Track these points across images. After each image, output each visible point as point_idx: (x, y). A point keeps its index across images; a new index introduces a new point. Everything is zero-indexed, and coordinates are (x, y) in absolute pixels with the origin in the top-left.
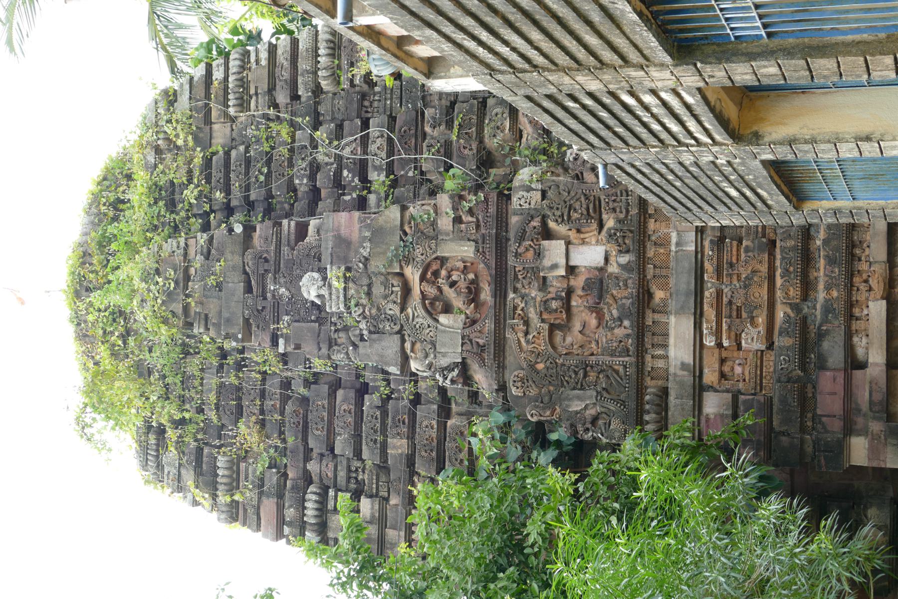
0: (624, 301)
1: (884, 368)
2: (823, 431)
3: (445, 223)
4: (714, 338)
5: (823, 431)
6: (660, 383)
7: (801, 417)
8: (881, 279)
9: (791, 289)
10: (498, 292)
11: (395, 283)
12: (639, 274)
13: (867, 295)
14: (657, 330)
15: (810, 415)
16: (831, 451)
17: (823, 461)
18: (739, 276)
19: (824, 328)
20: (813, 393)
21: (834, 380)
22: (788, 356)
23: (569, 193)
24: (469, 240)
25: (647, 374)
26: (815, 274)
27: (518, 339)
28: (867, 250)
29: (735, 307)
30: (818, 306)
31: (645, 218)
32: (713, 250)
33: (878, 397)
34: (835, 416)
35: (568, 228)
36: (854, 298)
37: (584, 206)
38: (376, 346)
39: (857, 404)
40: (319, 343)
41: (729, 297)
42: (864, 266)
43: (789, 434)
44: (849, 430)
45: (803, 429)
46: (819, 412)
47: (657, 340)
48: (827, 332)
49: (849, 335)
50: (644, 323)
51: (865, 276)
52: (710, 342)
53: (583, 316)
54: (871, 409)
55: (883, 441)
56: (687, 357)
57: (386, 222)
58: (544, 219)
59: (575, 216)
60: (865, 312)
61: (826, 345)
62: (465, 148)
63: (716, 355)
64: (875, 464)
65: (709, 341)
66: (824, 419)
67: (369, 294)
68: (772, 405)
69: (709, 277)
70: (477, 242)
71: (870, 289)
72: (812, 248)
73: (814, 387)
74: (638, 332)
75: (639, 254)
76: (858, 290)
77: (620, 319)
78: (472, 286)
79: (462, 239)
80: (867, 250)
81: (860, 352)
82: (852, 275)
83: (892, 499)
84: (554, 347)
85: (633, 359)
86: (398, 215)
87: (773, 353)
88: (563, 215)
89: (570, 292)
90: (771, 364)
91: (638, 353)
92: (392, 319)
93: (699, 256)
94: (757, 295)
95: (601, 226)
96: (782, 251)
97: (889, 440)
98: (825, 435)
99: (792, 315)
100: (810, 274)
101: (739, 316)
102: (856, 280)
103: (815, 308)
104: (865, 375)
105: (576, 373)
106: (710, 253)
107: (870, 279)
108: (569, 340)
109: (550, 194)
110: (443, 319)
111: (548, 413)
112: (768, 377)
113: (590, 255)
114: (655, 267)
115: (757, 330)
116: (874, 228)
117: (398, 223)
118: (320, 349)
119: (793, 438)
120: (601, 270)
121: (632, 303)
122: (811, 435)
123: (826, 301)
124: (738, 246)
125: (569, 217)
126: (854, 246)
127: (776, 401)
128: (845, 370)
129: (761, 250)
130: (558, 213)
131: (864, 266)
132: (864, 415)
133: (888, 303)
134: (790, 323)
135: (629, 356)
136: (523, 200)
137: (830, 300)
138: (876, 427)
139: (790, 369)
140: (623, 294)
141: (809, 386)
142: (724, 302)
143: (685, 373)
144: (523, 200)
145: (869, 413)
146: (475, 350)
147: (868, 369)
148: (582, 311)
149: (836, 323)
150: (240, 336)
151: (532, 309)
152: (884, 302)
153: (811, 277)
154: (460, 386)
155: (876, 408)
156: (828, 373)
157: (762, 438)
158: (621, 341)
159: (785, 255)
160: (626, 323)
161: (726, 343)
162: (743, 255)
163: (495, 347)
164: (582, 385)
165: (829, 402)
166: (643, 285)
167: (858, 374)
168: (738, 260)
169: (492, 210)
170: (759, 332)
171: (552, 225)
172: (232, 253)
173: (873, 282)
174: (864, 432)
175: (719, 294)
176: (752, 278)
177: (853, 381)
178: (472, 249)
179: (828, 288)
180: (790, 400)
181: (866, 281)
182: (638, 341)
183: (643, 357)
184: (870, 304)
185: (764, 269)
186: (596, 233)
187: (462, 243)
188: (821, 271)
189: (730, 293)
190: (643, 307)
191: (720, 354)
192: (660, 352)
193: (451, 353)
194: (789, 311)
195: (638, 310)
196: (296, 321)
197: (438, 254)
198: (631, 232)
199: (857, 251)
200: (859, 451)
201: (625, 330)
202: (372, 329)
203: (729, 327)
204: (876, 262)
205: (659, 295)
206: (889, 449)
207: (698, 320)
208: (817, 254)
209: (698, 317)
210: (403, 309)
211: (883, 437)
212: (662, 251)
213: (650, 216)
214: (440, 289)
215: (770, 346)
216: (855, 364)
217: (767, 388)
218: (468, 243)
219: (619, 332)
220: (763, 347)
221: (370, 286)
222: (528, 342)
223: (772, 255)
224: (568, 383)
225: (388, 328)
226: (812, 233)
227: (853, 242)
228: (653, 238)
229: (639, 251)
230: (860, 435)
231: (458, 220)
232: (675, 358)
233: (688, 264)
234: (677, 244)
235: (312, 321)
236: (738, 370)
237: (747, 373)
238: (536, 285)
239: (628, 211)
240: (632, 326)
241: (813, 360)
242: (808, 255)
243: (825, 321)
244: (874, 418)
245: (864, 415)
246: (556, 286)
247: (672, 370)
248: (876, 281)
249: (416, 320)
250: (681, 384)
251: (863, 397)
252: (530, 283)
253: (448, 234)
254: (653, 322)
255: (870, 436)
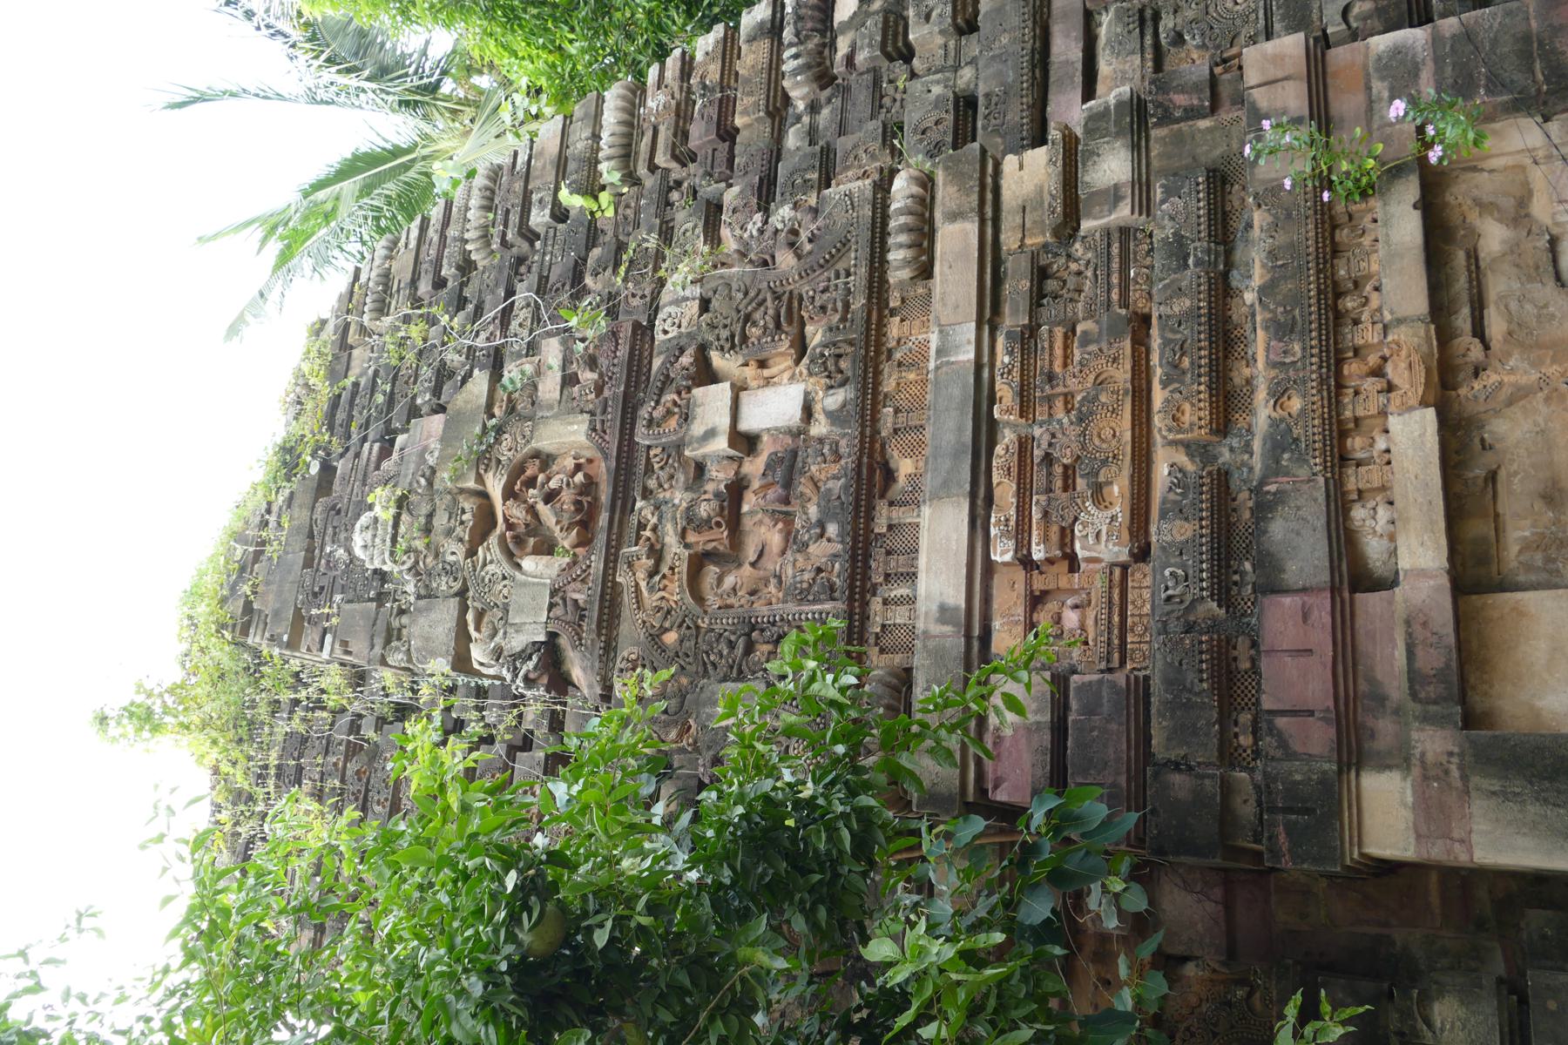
0: (830, 484)
1: (1445, 581)
2: (1279, 754)
3: (550, 387)
4: (1011, 544)
5: (1279, 754)
6: (898, 659)
7: (1220, 721)
8: (1415, 358)
9: (1187, 407)
10: (619, 503)
11: (467, 506)
12: (863, 426)
13: (1382, 399)
14: (895, 542)
15: (1245, 718)
16: (1308, 811)
17: (1282, 838)
18: (1068, 397)
19: (1272, 488)
20: (1253, 661)
21: (1305, 617)
22: (1184, 567)
23: (746, 294)
24: (582, 412)
25: (872, 640)
26: (1247, 372)
27: (637, 585)
28: (1374, 296)
29: (1058, 470)
30: (1257, 445)
31: (881, 317)
32: (1011, 353)
33: (1432, 660)
34: (1311, 713)
35: (741, 360)
36: (1348, 414)
37: (771, 312)
38: (422, 620)
39: (1372, 681)
40: (372, 637)
41: (1045, 445)
42: (1368, 335)
43: (1190, 768)
44: (1354, 752)
45: (1228, 755)
46: (1267, 703)
47: (897, 564)
48: (1280, 497)
49: (1339, 505)
50: (869, 530)
51: (1373, 360)
52: (1002, 553)
53: (763, 534)
54: (1414, 695)
55: (1459, 784)
56: (951, 592)
57: (466, 402)
58: (703, 350)
59: (754, 332)
60: (1381, 444)
61: (1277, 529)
62: (634, 296)
63: (1020, 587)
64: (1436, 852)
65: (1002, 553)
66: (1281, 722)
67: (427, 530)
68: (1147, 695)
69: (1005, 410)
70: (592, 413)
71: (1390, 388)
72: (1237, 313)
73: (1254, 644)
74: (854, 548)
75: (865, 387)
76: (1357, 393)
77: (821, 525)
78: (585, 500)
79: (571, 411)
80: (1374, 296)
81: (1374, 549)
82: (1340, 362)
83: (1500, 981)
84: (699, 599)
85: (841, 606)
86: (485, 387)
87: (1147, 568)
88: (733, 336)
89: (737, 489)
90: (1147, 594)
91: (852, 593)
92: (451, 571)
93: (986, 374)
94: (1107, 433)
95: (801, 347)
96: (1162, 329)
97: (1475, 780)
98: (1286, 765)
99: (1190, 467)
100: (1234, 374)
101: (1068, 486)
102: (1352, 369)
103: (1248, 449)
104: (1391, 602)
105: (731, 645)
106: (1007, 359)
107: (1389, 368)
108: (729, 581)
109: (715, 304)
110: (528, 563)
111: (673, 734)
112: (1139, 629)
113: (775, 406)
114: (897, 411)
115: (1109, 513)
116: (1387, 243)
117: (483, 400)
118: (372, 647)
119: (1203, 777)
120: (797, 433)
121: (846, 488)
122: (1251, 771)
123: (1274, 423)
124: (1066, 337)
125: (745, 338)
126: (1338, 295)
127: (1156, 684)
128: (1334, 590)
129: (1114, 333)
130: (725, 334)
131: (1368, 335)
132: (1397, 712)
133: (1439, 414)
134: (1185, 487)
135: (833, 599)
136: (669, 321)
137: (1282, 420)
138: (1434, 742)
139: (1189, 598)
140: (829, 477)
141: (1243, 643)
142: (1036, 461)
143: (948, 629)
144: (669, 321)
145: (1411, 705)
146: (569, 618)
147: (1397, 590)
148: (761, 522)
149: (1303, 473)
150: (285, 638)
151: (669, 527)
152: (1430, 413)
153: (1238, 381)
154: (542, 691)
155: (1431, 690)
156: (1287, 600)
157: (1122, 780)
158: (819, 570)
159: (1170, 336)
160: (832, 529)
161: (1038, 554)
162: (1077, 352)
163: (601, 608)
164: (740, 672)
165: (1294, 674)
166: (872, 448)
167: (1370, 603)
168: (1065, 365)
169: (623, 352)
170: (1114, 518)
171: (717, 359)
172: (300, 506)
173: (1396, 372)
174: (1399, 758)
175: (1024, 445)
176: (1096, 398)
177: (1360, 622)
178: (585, 427)
179: (1279, 395)
180: (1191, 677)
181: (1378, 372)
182: (853, 567)
183: (865, 604)
184: (1394, 422)
185: (1122, 375)
186: (790, 362)
187: (571, 418)
188: (1260, 359)
189: (1047, 437)
190: (870, 496)
191: (1029, 583)
192: (901, 591)
193: (529, 629)
194: (1182, 459)
195: (857, 500)
196: (349, 601)
197: (534, 444)
198: (851, 343)
199: (1349, 303)
200: (1386, 817)
201: (827, 549)
202: (423, 592)
203: (1046, 514)
204: (1400, 321)
205: (905, 467)
206: (1478, 806)
207: (981, 511)
208: (1248, 327)
209: (980, 502)
210: (471, 553)
211: (1455, 773)
212: (912, 376)
213: (893, 312)
214: (532, 510)
215: (1142, 554)
216: (1355, 576)
217: (1138, 655)
218: (580, 417)
219: (819, 551)
220: (1124, 557)
221: (430, 516)
222: (651, 589)
223: (1140, 342)
224: (714, 665)
225: (444, 587)
226: (1234, 284)
227: (1335, 284)
228: (898, 355)
229: (865, 379)
230: (1389, 767)
231: (569, 380)
232: (928, 597)
233: (960, 391)
234: (939, 352)
235: (370, 600)
236: (1071, 619)
237: (1090, 622)
238: (682, 478)
239: (847, 305)
240: (841, 534)
241: (1251, 578)
242: (1226, 333)
243: (1274, 468)
244: (1426, 719)
245: (1397, 712)
246: (719, 476)
247: (920, 625)
248: (1403, 365)
249: (488, 568)
250: (938, 655)
251: (1389, 661)
252: (672, 477)
253: (550, 407)
254: (890, 527)
255: (1416, 771)
